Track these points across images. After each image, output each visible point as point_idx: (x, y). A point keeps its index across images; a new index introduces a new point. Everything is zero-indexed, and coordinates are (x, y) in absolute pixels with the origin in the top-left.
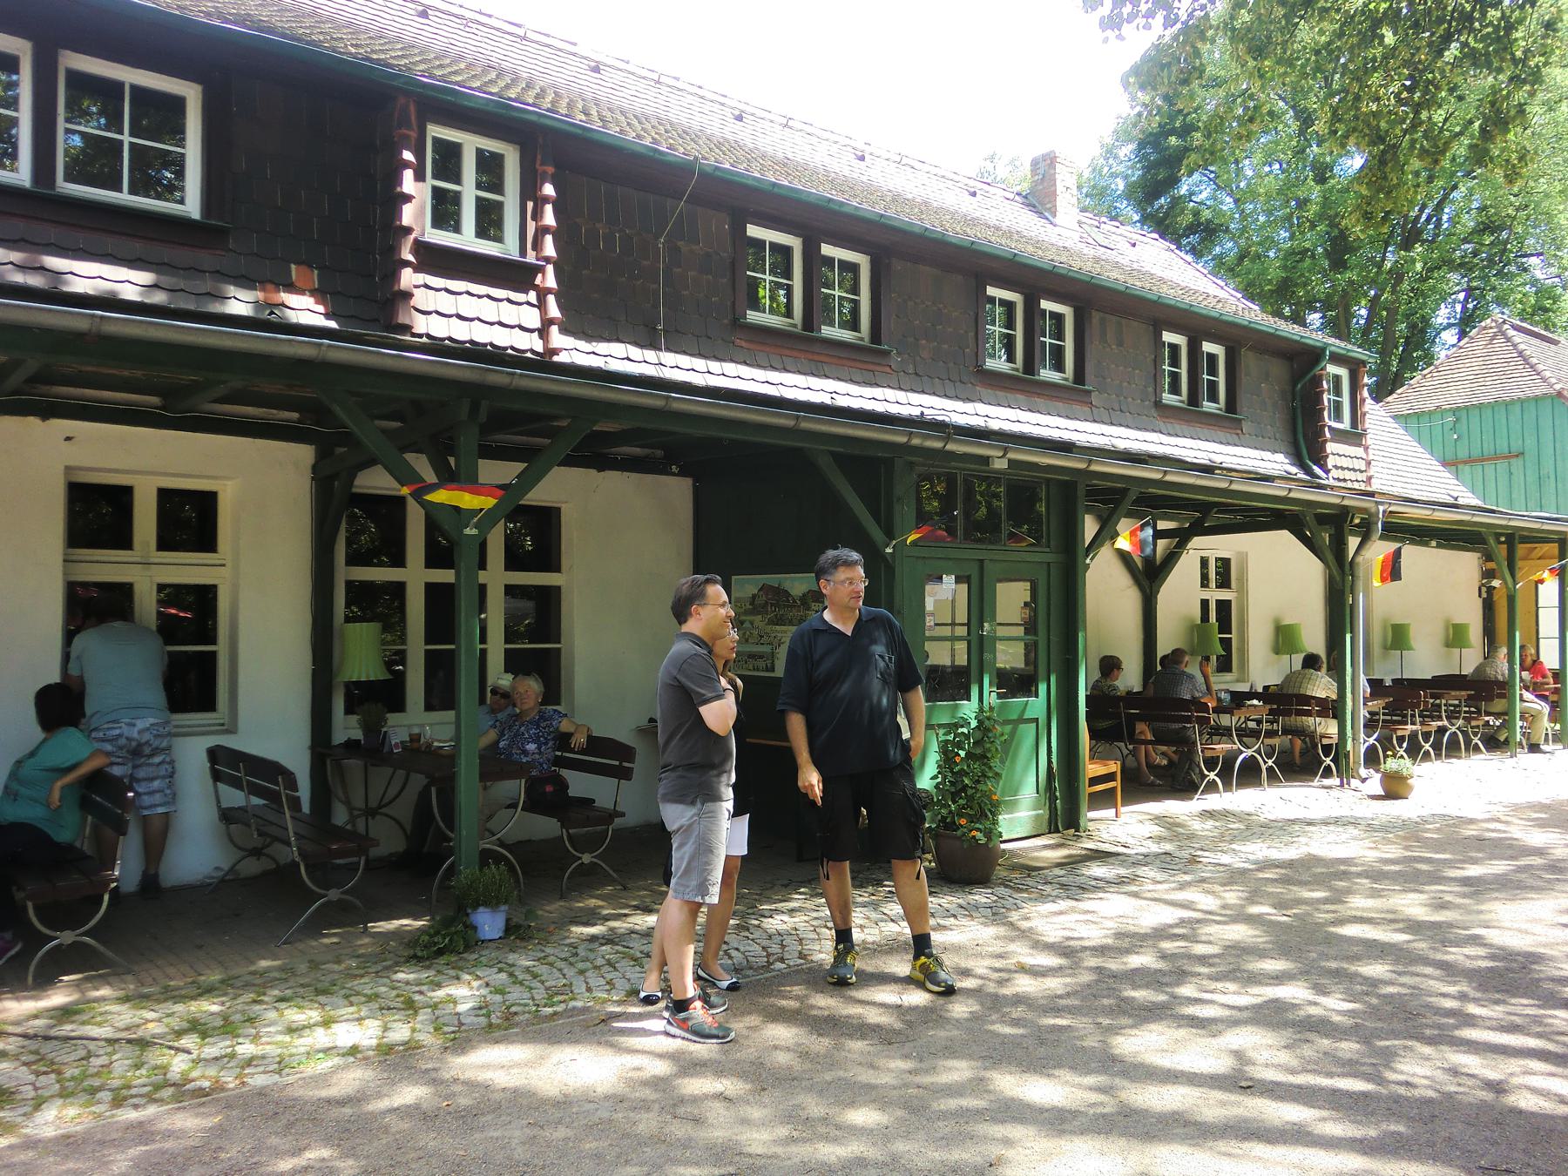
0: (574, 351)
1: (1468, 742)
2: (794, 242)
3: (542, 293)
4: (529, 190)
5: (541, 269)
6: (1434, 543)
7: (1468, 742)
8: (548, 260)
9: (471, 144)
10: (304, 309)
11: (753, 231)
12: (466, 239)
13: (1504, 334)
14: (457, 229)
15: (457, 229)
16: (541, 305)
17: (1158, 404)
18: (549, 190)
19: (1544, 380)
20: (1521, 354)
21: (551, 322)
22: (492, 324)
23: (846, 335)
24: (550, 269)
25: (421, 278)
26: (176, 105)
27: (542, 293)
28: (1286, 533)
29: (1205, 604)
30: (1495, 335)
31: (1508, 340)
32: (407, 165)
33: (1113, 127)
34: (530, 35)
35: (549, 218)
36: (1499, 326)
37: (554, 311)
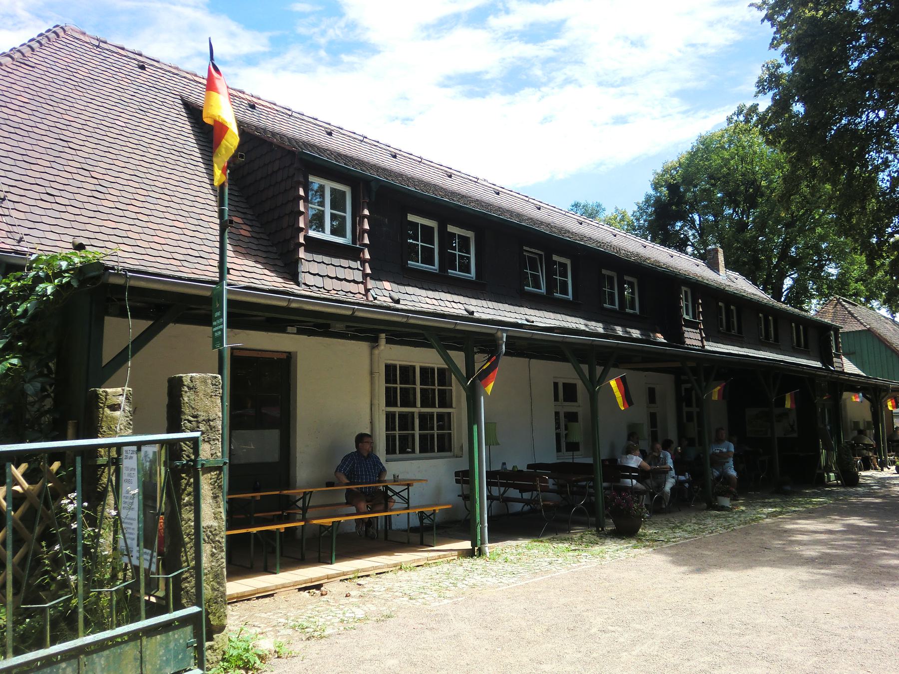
0: (711, 346)
1: (29, 613)
2: (470, 234)
3: (701, 329)
4: (356, 213)
5: (363, 250)
6: (294, 330)
7: (29, 613)
8: (365, 245)
9: (329, 185)
10: (660, 338)
11: (411, 218)
12: (326, 236)
13: (840, 303)
14: (323, 231)
15: (323, 231)
16: (701, 334)
17: (719, 332)
18: (366, 212)
19: (862, 323)
20: (849, 312)
21: (368, 275)
22: (314, 275)
23: (631, 311)
24: (366, 251)
25: (309, 256)
26: (565, 265)
27: (701, 329)
28: (171, 325)
29: (557, 414)
30: (836, 304)
31: (843, 306)
32: (301, 197)
33: (641, 199)
34: (294, 114)
35: (367, 226)
36: (838, 300)
37: (368, 271)
